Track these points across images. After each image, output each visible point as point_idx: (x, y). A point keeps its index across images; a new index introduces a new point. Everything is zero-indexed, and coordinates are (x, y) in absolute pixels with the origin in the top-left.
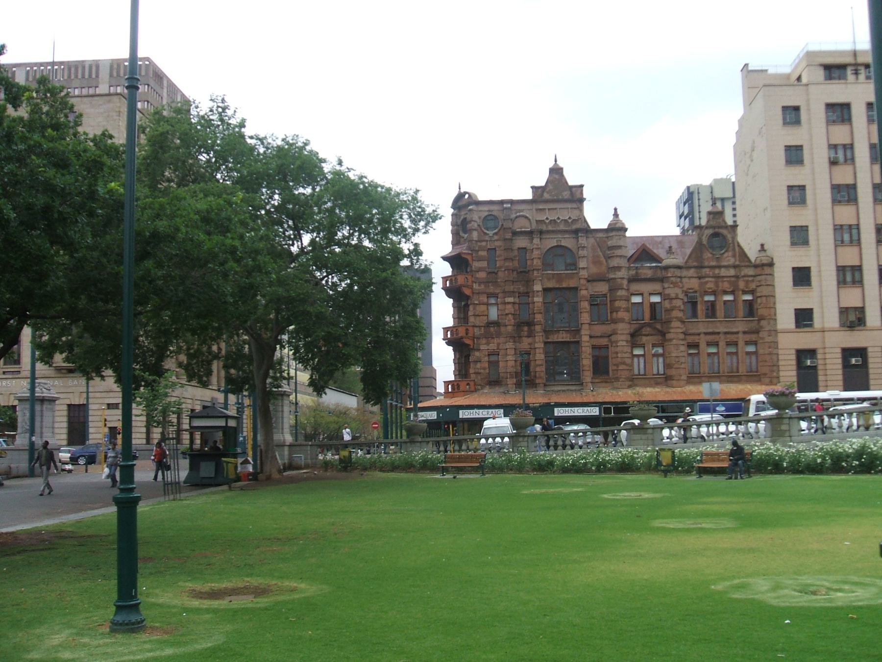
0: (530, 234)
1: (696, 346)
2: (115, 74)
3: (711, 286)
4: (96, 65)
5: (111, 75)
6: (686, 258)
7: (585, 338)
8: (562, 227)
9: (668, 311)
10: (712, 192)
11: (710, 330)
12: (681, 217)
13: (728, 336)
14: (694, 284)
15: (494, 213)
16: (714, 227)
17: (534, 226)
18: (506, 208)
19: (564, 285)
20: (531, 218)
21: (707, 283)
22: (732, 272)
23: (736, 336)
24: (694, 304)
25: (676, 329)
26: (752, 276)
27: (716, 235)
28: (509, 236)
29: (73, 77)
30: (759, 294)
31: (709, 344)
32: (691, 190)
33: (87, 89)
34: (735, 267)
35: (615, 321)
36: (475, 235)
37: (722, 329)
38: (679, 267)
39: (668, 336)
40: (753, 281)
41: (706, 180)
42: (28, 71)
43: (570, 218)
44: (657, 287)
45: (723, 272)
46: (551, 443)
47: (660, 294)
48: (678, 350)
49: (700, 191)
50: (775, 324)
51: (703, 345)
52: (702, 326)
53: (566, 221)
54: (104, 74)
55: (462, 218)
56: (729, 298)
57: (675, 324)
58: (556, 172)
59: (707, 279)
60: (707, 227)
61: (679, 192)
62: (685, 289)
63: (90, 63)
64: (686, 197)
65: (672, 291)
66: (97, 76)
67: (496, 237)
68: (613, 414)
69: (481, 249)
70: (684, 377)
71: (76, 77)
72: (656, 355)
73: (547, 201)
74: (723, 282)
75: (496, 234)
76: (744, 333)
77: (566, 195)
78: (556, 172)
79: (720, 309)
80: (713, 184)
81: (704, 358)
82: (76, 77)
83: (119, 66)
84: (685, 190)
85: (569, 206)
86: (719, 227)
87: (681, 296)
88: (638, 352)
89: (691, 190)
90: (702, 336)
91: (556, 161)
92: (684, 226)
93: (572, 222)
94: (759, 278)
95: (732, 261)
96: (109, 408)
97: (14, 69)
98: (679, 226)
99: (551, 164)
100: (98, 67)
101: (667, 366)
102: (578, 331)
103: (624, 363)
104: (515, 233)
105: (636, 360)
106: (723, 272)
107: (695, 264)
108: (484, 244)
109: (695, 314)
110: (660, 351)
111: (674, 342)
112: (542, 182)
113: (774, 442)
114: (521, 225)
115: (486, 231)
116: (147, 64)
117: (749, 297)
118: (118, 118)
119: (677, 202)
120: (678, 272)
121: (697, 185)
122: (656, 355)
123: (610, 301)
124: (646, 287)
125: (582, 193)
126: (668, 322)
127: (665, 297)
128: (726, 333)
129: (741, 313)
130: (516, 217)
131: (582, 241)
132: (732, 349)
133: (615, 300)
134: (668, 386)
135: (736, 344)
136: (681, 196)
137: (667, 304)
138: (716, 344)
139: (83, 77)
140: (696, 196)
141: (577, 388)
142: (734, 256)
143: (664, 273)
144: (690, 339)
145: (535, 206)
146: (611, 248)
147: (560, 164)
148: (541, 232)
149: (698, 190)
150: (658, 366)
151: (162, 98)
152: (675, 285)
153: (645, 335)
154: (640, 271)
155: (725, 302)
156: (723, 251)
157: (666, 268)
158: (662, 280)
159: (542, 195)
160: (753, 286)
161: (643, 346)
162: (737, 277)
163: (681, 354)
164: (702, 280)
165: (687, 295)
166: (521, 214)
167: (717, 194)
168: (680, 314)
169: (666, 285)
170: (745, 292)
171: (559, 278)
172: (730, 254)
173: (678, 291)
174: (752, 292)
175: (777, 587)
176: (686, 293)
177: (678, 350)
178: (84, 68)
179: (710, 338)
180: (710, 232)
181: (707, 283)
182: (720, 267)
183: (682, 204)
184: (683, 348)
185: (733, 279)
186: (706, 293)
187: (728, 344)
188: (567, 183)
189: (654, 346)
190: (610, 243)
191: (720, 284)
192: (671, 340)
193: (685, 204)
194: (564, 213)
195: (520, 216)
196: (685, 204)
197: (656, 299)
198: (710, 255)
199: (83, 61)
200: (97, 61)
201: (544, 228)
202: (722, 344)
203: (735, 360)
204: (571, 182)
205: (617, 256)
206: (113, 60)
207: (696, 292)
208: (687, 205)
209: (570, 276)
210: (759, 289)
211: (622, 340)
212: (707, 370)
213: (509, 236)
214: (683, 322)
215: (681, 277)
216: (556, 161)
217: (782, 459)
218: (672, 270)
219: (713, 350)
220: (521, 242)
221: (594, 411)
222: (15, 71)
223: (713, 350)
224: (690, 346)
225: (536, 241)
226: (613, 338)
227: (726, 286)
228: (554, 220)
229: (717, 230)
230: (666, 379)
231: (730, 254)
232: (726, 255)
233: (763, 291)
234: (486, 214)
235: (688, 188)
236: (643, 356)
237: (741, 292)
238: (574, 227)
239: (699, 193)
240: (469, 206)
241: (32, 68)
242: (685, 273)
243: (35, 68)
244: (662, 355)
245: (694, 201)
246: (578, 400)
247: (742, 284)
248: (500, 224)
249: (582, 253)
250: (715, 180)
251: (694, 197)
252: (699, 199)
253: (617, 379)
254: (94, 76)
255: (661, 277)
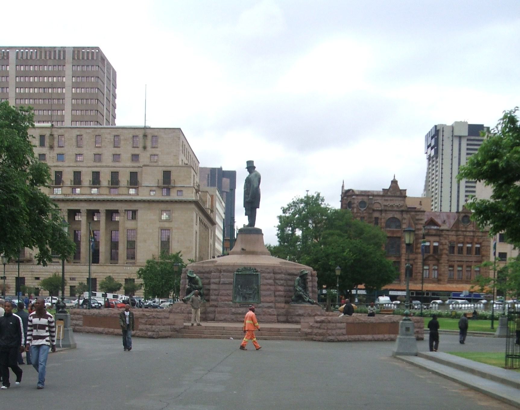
0: (381, 211)
1: (452, 266)
2: (76, 58)
3: (461, 239)
4: (63, 50)
5: (74, 59)
6: (452, 226)
7: (403, 260)
8: (395, 209)
9: (442, 250)
10: (453, 131)
11: (459, 260)
12: (428, 147)
13: (468, 263)
14: (454, 238)
15: (364, 200)
16: (465, 213)
17: (383, 208)
18: (370, 199)
19: (395, 236)
20: (381, 203)
21: (460, 238)
22: (472, 234)
23: (471, 263)
24: (454, 247)
25: (444, 258)
26: (480, 236)
27: (466, 216)
28: (371, 211)
29: (48, 58)
30: (483, 245)
31: (459, 266)
32: (438, 128)
33: (57, 67)
34: (473, 232)
35: (417, 253)
36: (355, 210)
37: (465, 260)
38: (448, 230)
39: (440, 261)
40: (481, 239)
41: (449, 122)
42: (17, 52)
43: (399, 205)
44: (437, 238)
45: (468, 234)
46: (412, 307)
47: (438, 242)
48: (445, 268)
49: (444, 130)
50: (489, 259)
51: (456, 266)
52: (456, 257)
53: (397, 206)
54: (69, 57)
55: (349, 201)
56: (469, 245)
57: (444, 256)
58: (394, 182)
59: (460, 236)
60: (462, 213)
61: (429, 128)
62: (450, 240)
63: (59, 49)
64: (433, 133)
65: (444, 241)
66: (64, 58)
67: (365, 212)
68: (415, 295)
69: (357, 216)
70: (446, 280)
71: (50, 58)
72: (434, 270)
73: (389, 196)
74: (467, 238)
75: (365, 210)
76: (475, 262)
77: (398, 194)
78: (394, 182)
79: (465, 250)
80: (454, 125)
81: (456, 273)
82: (50, 58)
83: (78, 51)
84: (433, 128)
85: (400, 199)
86: (467, 213)
87: (448, 243)
88: (426, 267)
89: (438, 128)
90: (456, 262)
91: (394, 177)
92: (430, 154)
93: (400, 207)
94: (484, 237)
95: (472, 229)
96: (70, 280)
97: (8, 50)
98: (426, 153)
99: (392, 179)
100: (64, 52)
101: (439, 275)
102: (400, 257)
103: (420, 273)
104: (374, 210)
105: (425, 271)
106: (468, 234)
107: (455, 229)
108: (359, 214)
109: (453, 253)
110: (436, 267)
111: (443, 264)
112: (387, 187)
113: (485, 311)
114: (376, 207)
115: (360, 209)
116: (97, 52)
117: (478, 246)
118: (178, 140)
119: (426, 136)
120: (447, 233)
121: (443, 125)
122: (434, 270)
123: (416, 244)
124: (432, 239)
125: (405, 193)
126: (441, 255)
127: (440, 244)
128: (467, 261)
129: (474, 253)
130: (375, 203)
131: (405, 216)
132: (469, 269)
133: (418, 244)
134: (439, 284)
135: (470, 267)
136: (430, 132)
137: (441, 247)
138: (462, 266)
139: (55, 58)
140: (441, 134)
141: (399, 282)
142: (473, 227)
143: (441, 233)
144: (450, 263)
145: (384, 198)
146: (418, 220)
147: (397, 179)
148: (386, 211)
149: (443, 128)
150: (435, 274)
151: (104, 73)
152: (446, 238)
153: (430, 260)
154: (430, 231)
155: (468, 247)
156: (468, 224)
157: (442, 230)
158: (439, 236)
159: (387, 193)
160: (481, 241)
161: (428, 265)
162: (474, 236)
163: (446, 270)
164: (458, 237)
165: (450, 243)
166: (377, 201)
167: (456, 133)
168: (447, 252)
169: (441, 238)
170: (477, 243)
171: (393, 232)
172: (472, 225)
173: (447, 241)
174: (480, 244)
175: (494, 131)
176: (450, 242)
177: (445, 268)
178: (55, 51)
179: (459, 263)
180: (463, 215)
181: (460, 238)
182: (466, 231)
183: (430, 137)
184: (446, 267)
185: (472, 237)
186: (459, 243)
187: (468, 267)
188: (399, 188)
189: (434, 265)
190: (417, 217)
191: (466, 239)
192: (441, 263)
193: (432, 138)
194: (397, 202)
195: (376, 202)
196: (432, 138)
197: (436, 244)
198: (462, 226)
199: (55, 48)
200: (64, 48)
201: (387, 208)
202: (464, 266)
203: (469, 274)
204: (401, 188)
205: (420, 224)
206: (74, 48)
207: (454, 242)
208: (433, 140)
209: (398, 232)
210: (484, 242)
211: (420, 262)
212: (457, 277)
213: (371, 211)
214: (448, 255)
215: (448, 235)
216: (394, 177)
217: (487, 316)
218: (445, 232)
219: (460, 269)
220: (376, 215)
221: (404, 293)
222: (8, 52)
223: (460, 269)
224: (450, 266)
225: (383, 215)
226: (416, 261)
227: (468, 240)
228: (392, 205)
229: (466, 214)
230: (438, 281)
231: (472, 225)
232: (469, 226)
233: (485, 243)
234: (361, 200)
235: (436, 126)
236: (429, 269)
237: (475, 243)
238: (401, 209)
239: (443, 131)
240: (353, 196)
241: (20, 50)
242: (450, 233)
243: (22, 50)
244: (437, 270)
245: (439, 137)
246: (399, 288)
247: (476, 240)
248: (367, 205)
249: (404, 221)
250: (456, 122)
251: (439, 134)
252: (443, 136)
253: (416, 279)
254: (62, 58)
255: (439, 234)
